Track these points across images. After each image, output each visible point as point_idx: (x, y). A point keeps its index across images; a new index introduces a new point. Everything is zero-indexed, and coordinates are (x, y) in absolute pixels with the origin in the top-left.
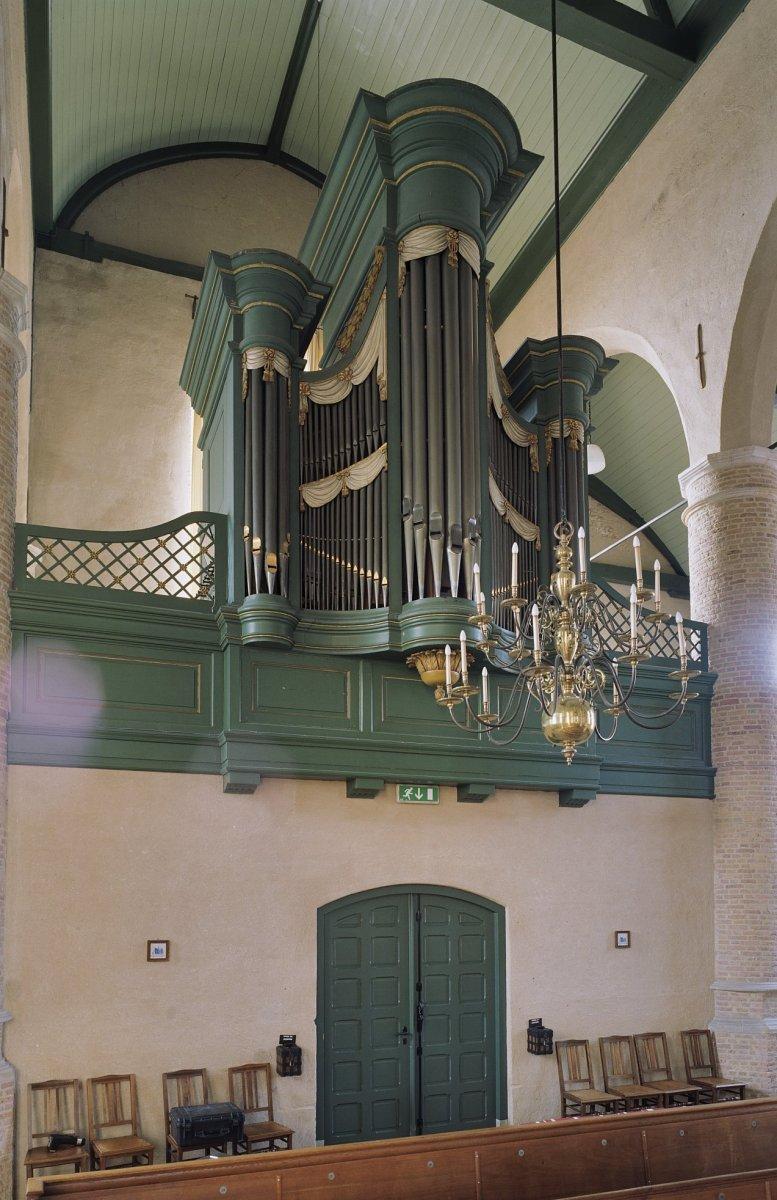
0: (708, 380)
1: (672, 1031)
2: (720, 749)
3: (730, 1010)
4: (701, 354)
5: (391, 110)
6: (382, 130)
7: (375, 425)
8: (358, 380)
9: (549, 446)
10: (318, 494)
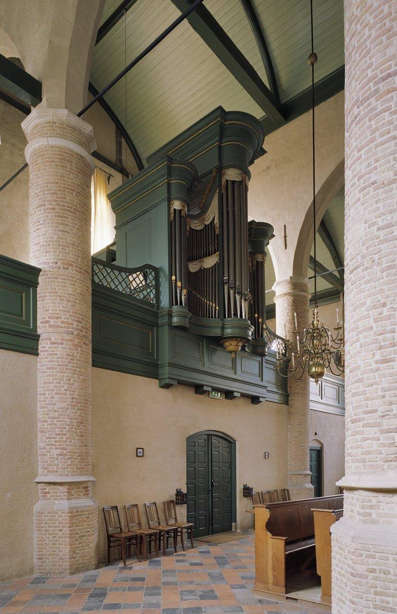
0: (288, 247)
1: (279, 489)
2: (290, 387)
3: (293, 481)
4: (285, 237)
5: (228, 117)
6: (222, 123)
7: (213, 243)
8: (207, 223)
9: (255, 264)
10: (194, 267)
